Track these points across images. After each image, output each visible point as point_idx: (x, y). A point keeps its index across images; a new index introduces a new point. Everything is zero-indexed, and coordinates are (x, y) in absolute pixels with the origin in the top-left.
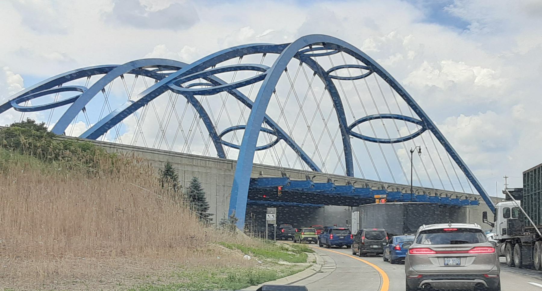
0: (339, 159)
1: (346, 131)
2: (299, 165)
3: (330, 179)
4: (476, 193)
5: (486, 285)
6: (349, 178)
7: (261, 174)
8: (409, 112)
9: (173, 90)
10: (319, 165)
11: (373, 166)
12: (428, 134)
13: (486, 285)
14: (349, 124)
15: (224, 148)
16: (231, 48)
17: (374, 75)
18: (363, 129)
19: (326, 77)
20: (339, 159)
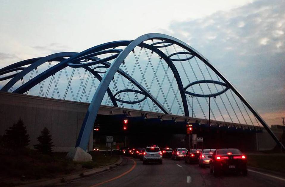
0: (180, 106)
1: (183, 91)
2: (160, 111)
3: (174, 117)
4: (261, 125)
5: (178, 165)
6: (187, 117)
7: (111, 113)
8: (216, 78)
9: (71, 66)
10: (168, 110)
11: (200, 110)
12: (229, 91)
13: (178, 165)
14: (184, 87)
15: (262, 125)
16: (206, 59)
17: (168, 54)
18: (196, 89)
19: (168, 60)
20: (180, 106)
